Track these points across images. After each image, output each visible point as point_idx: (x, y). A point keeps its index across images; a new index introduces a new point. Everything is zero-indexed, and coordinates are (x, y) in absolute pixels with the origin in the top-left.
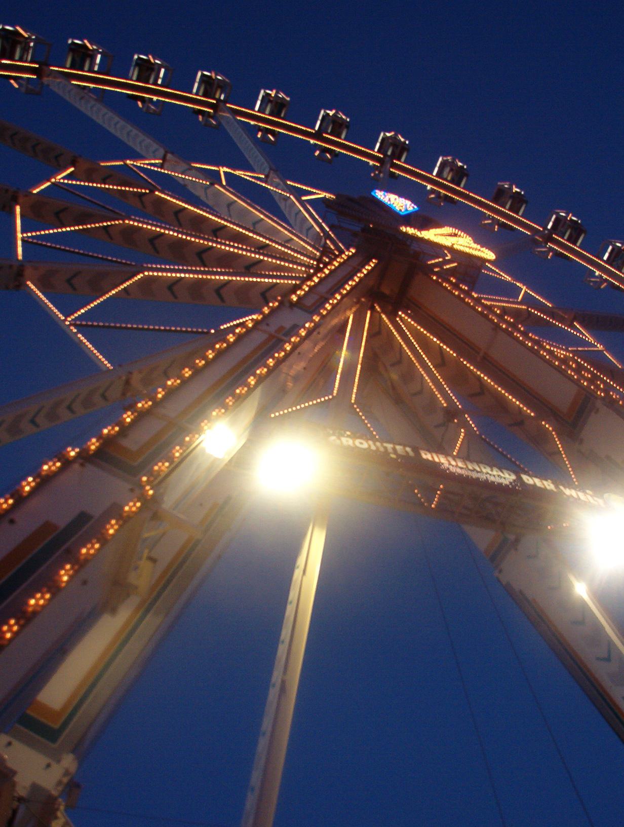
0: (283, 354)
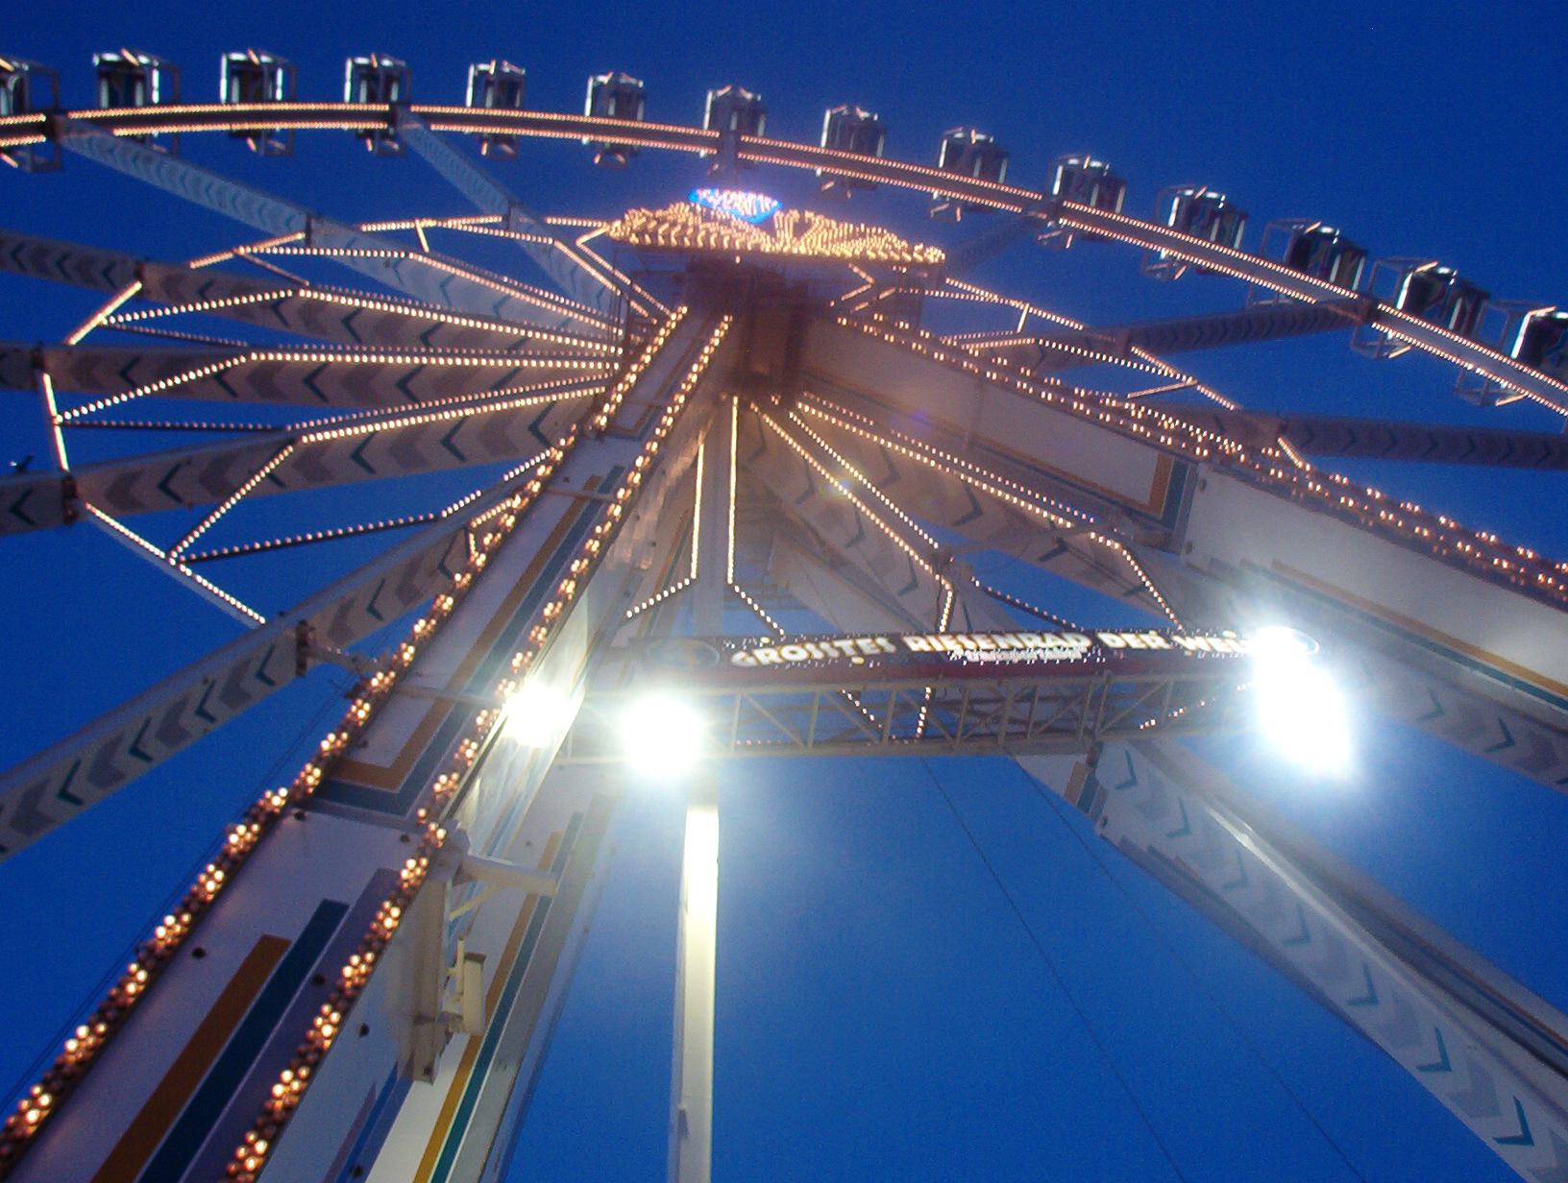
0: (609, 525)
